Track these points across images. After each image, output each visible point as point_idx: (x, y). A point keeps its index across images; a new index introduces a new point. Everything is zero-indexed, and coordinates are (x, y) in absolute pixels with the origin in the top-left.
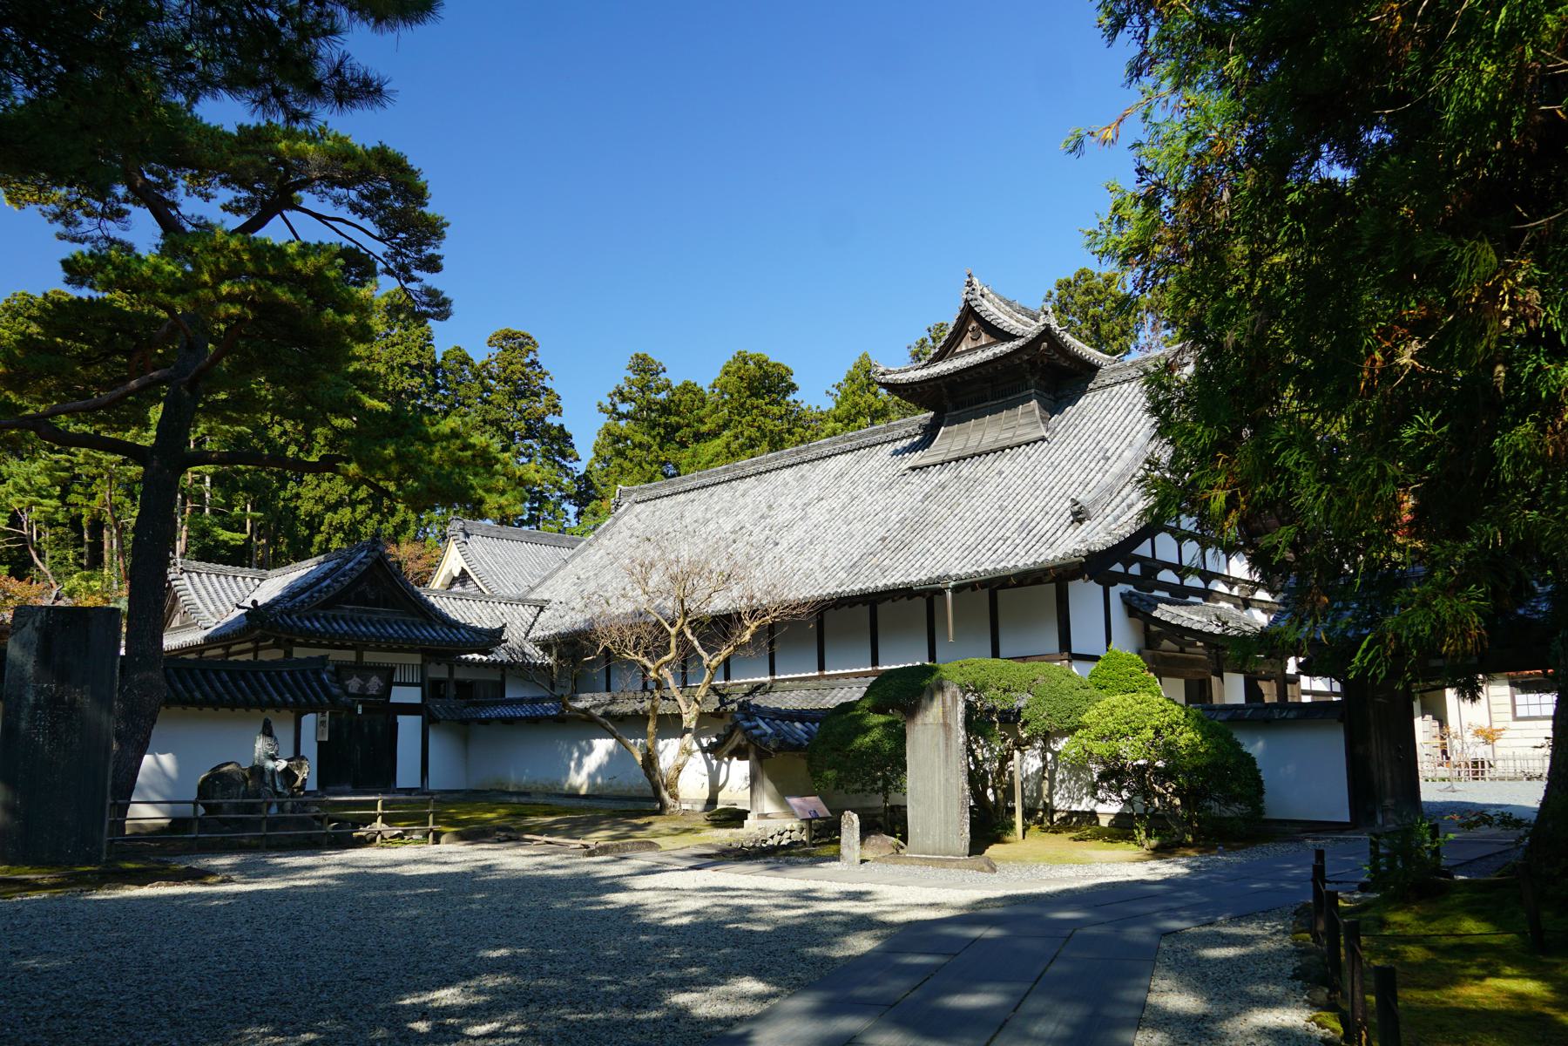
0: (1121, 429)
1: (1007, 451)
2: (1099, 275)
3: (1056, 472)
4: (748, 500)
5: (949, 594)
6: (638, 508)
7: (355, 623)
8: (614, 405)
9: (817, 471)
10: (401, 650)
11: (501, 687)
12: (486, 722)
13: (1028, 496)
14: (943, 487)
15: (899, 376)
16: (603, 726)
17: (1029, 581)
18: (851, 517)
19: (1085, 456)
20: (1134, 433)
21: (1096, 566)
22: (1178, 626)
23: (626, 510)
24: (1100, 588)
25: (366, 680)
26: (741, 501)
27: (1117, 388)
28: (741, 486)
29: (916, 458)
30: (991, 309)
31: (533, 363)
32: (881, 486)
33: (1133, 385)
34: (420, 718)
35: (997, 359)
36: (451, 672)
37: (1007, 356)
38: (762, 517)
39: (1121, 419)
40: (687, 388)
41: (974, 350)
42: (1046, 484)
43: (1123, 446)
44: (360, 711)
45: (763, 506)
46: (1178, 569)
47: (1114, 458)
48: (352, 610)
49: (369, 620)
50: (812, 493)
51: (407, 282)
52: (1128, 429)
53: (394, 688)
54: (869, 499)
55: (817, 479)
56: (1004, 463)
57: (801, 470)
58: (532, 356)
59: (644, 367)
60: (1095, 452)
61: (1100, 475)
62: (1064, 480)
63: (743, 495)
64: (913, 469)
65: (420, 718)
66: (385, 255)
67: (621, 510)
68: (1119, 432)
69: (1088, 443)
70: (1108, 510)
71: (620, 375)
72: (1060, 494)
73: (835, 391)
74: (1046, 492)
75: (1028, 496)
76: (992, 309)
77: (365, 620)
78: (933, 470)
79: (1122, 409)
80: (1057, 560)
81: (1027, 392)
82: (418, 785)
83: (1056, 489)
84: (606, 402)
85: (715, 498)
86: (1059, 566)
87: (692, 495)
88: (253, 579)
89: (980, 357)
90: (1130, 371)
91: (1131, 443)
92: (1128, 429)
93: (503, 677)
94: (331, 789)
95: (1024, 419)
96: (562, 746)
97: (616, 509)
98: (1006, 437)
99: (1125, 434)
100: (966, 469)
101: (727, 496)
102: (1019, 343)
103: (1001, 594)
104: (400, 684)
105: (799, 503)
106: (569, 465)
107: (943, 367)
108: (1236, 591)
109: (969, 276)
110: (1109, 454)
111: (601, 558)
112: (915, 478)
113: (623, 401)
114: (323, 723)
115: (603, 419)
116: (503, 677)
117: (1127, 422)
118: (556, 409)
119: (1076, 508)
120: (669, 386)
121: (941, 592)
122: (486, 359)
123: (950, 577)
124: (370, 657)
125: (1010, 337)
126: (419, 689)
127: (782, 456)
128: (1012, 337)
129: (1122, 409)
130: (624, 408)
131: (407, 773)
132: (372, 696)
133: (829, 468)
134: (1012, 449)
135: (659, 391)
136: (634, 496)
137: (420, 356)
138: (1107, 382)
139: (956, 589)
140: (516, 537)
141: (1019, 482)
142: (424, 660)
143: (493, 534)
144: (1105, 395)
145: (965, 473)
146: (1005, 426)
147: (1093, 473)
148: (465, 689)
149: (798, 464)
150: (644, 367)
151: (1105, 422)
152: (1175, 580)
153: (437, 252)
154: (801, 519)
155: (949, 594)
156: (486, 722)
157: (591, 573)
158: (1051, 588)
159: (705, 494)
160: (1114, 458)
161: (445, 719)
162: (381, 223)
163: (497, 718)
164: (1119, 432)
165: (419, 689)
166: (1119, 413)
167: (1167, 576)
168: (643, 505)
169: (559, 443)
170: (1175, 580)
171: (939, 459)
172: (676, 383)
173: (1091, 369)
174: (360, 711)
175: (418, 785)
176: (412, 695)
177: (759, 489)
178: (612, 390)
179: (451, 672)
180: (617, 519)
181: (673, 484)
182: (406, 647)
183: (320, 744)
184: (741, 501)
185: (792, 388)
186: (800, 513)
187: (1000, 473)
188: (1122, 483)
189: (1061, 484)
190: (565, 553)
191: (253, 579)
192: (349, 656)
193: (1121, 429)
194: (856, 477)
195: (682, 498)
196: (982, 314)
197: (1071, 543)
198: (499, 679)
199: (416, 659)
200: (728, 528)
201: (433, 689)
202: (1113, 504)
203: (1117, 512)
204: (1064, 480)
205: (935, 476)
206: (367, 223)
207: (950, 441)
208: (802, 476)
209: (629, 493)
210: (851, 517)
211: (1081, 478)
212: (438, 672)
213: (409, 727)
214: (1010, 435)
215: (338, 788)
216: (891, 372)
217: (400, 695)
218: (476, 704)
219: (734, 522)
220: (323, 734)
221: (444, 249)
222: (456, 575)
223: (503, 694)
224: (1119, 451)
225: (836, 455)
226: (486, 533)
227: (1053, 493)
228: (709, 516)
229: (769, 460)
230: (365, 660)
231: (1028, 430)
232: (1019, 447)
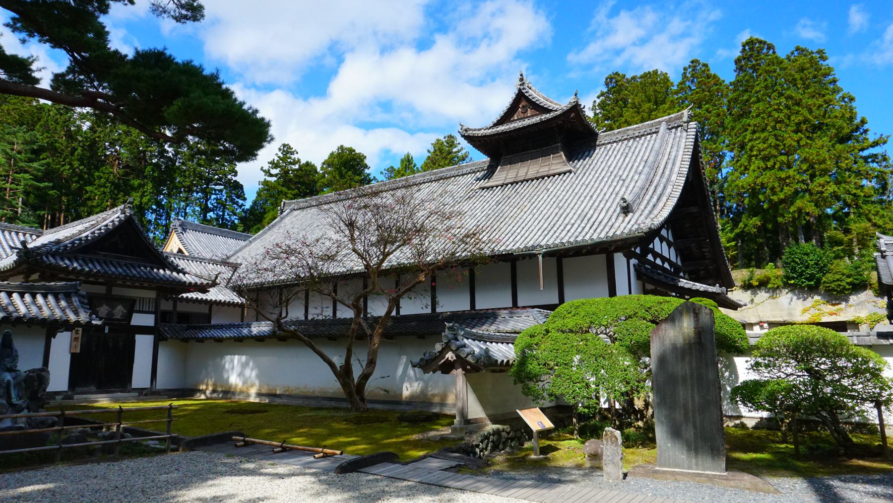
1: (546, 178)
5: (540, 257)
6: (295, 213)
7: (106, 264)
10: (142, 287)
11: (208, 317)
12: (201, 340)
16: (300, 339)
17: (584, 251)
21: (624, 245)
24: (625, 259)
25: (113, 307)
29: (483, 183)
30: (536, 94)
33: (620, 143)
35: (542, 122)
36: (175, 306)
37: (549, 120)
39: (559, 186)
41: (523, 119)
44: (106, 331)
48: (105, 256)
49: (118, 264)
53: (134, 315)
64: (483, 189)
67: (284, 214)
73: (384, 172)
74: (588, 198)
76: (535, 95)
77: (115, 263)
80: (625, 236)
81: (556, 145)
82: (148, 385)
86: (621, 240)
88: (31, 235)
89: (527, 122)
94: (79, 389)
95: (557, 162)
96: (218, 360)
97: (282, 213)
98: (544, 170)
102: (552, 115)
103: (565, 260)
104: (139, 312)
107: (501, 128)
114: (76, 339)
119: (625, 204)
120: (299, 161)
121: (535, 255)
123: (541, 246)
124: (117, 291)
126: (153, 316)
131: (140, 377)
132: (117, 320)
134: (549, 177)
138: (603, 142)
139: (545, 255)
142: (158, 295)
143: (199, 229)
146: (542, 165)
148: (184, 318)
155: (540, 257)
156: (201, 340)
158: (602, 258)
161: (171, 338)
163: (211, 338)
165: (153, 316)
171: (501, 182)
172: (303, 162)
174: (106, 331)
175: (148, 385)
176: (148, 320)
179: (175, 306)
182: (146, 285)
183: (74, 356)
190: (243, 243)
191: (31, 235)
192: (101, 290)
196: (530, 97)
197: (624, 227)
198: (208, 312)
199: (152, 294)
201: (162, 317)
205: (498, 194)
207: (502, 175)
209: (290, 204)
212: (166, 306)
213: (143, 344)
214: (547, 169)
215: (85, 389)
217: (138, 320)
218: (195, 328)
223: (210, 322)
226: (195, 229)
230: (113, 293)
231: (559, 167)
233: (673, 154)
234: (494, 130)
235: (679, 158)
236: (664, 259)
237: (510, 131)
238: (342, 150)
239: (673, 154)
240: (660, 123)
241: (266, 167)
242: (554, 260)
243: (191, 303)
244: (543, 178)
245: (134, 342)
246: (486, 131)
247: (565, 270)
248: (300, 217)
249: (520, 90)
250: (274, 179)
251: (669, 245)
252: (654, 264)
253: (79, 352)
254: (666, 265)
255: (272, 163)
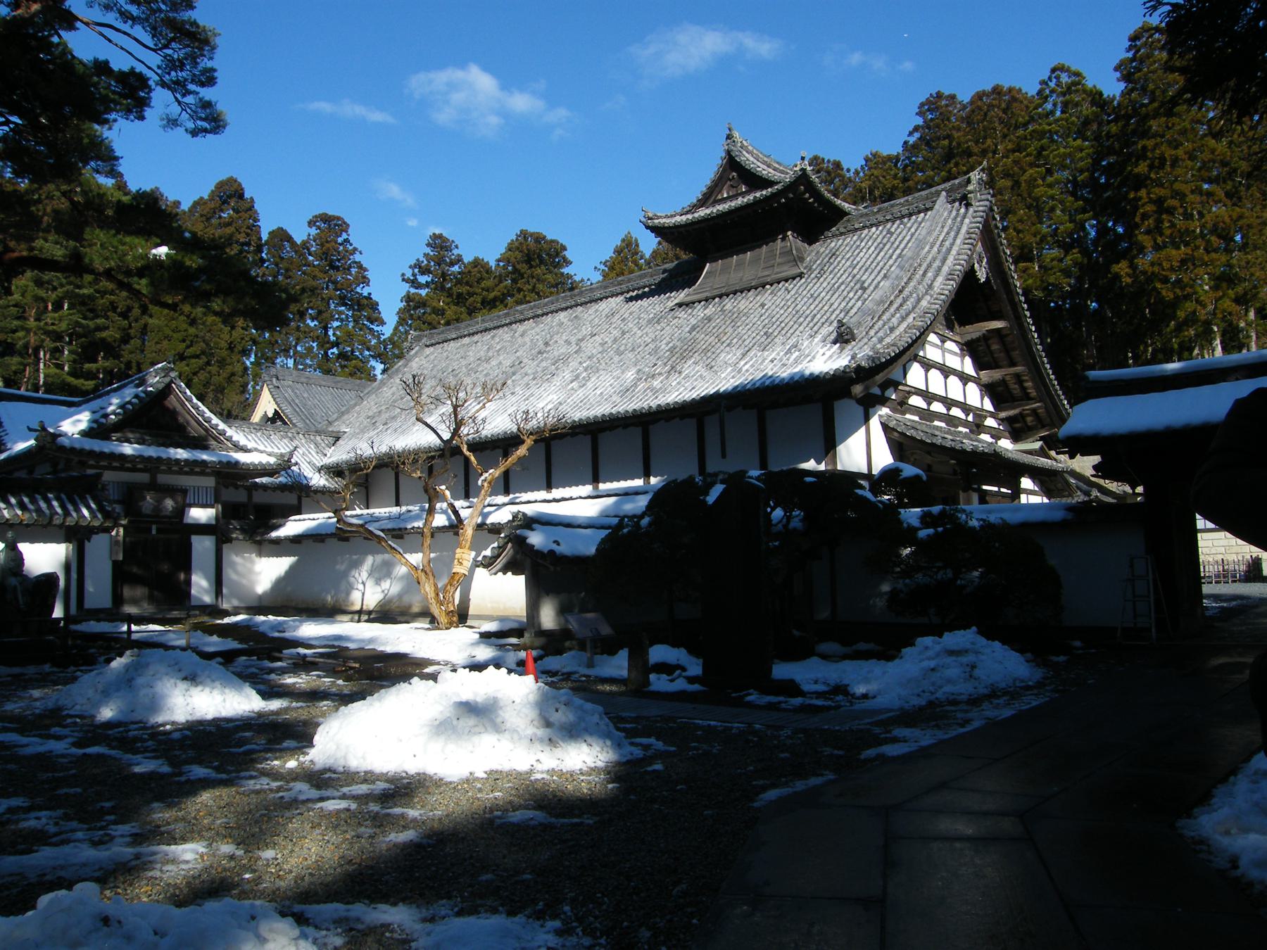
0: (875, 264)
2: (829, 161)
3: (817, 302)
4: (527, 339)
6: (428, 351)
8: (414, 275)
9: (590, 312)
13: (792, 323)
14: (709, 319)
15: (667, 221)
18: (622, 348)
19: (843, 287)
20: (887, 267)
22: (933, 445)
23: (416, 353)
26: (520, 340)
27: (866, 231)
28: (520, 328)
31: (347, 241)
32: (650, 321)
34: (523, 577)
35: (757, 202)
38: (540, 353)
39: (874, 256)
40: (477, 263)
42: (808, 312)
43: (879, 278)
44: (154, 532)
45: (541, 343)
46: (929, 397)
47: (872, 288)
50: (586, 330)
51: (184, 95)
52: (881, 264)
54: (639, 333)
55: (590, 319)
56: (766, 296)
57: (575, 312)
58: (345, 236)
59: (440, 244)
60: (852, 284)
61: (860, 303)
62: (826, 308)
63: (522, 336)
64: (680, 305)
65: (523, 577)
66: (159, 67)
68: (873, 266)
69: (844, 277)
70: (872, 333)
71: (420, 251)
72: (823, 320)
73: (603, 267)
74: (809, 319)
75: (792, 323)
78: (699, 306)
79: (873, 248)
83: (819, 316)
84: (409, 274)
85: (497, 340)
87: (476, 338)
89: (740, 201)
90: (877, 216)
91: (885, 276)
92: (881, 264)
93: (300, 499)
99: (879, 268)
100: (729, 304)
101: (507, 337)
105: (573, 339)
106: (376, 328)
107: (703, 212)
108: (970, 418)
109: (730, 129)
110: (866, 285)
111: (393, 394)
112: (682, 314)
113: (423, 273)
115: (406, 288)
116: (300, 499)
117: (879, 258)
118: (365, 281)
122: (305, 238)
124: (163, 479)
125: (767, 183)
127: (557, 300)
128: (777, 183)
129: (873, 248)
130: (423, 279)
133: (601, 309)
134: (771, 285)
135: (452, 264)
136: (424, 340)
137: (248, 235)
140: (324, 383)
141: (782, 312)
142: (217, 483)
144: (855, 238)
145: (729, 306)
147: (853, 301)
149: (571, 307)
150: (440, 244)
151: (858, 259)
152: (923, 405)
153: (210, 64)
154: (576, 352)
157: (383, 408)
159: (487, 336)
160: (872, 288)
162: (155, 33)
164: (873, 266)
166: (870, 251)
167: (916, 401)
168: (432, 349)
169: (366, 308)
170: (923, 405)
173: (841, 214)
174: (154, 532)
177: (537, 330)
178: (413, 262)
179: (250, 496)
180: (410, 360)
181: (459, 329)
184: (520, 340)
185: (568, 263)
186: (574, 348)
187: (763, 305)
188: (882, 308)
189: (822, 312)
193: (875, 264)
194: (626, 315)
195: (466, 340)
200: (508, 363)
202: (876, 327)
203: (881, 334)
204: (826, 308)
205: (700, 312)
206: (138, 31)
208: (576, 317)
209: (418, 339)
210: (622, 348)
211: (842, 306)
216: (659, 217)
219: (513, 358)
220: (117, 553)
221: (219, 61)
222: (270, 415)
224: (876, 282)
225: (607, 298)
227: (815, 320)
228: (490, 354)
229: (546, 305)
231: (785, 268)
232: (779, 283)
233: (947, 244)
234: (690, 217)
235: (954, 252)
236: (949, 403)
237: (669, 227)
238: (526, 239)
239: (947, 244)
240: (938, 194)
241: (409, 274)
242: (543, 445)
243: (269, 491)
244: (764, 287)
245: (190, 545)
246: (664, 220)
247: (554, 460)
248: (432, 357)
249: (729, 152)
250: (423, 292)
251: (965, 378)
252: (927, 415)
253: (121, 558)
254: (956, 412)
255: (418, 265)
